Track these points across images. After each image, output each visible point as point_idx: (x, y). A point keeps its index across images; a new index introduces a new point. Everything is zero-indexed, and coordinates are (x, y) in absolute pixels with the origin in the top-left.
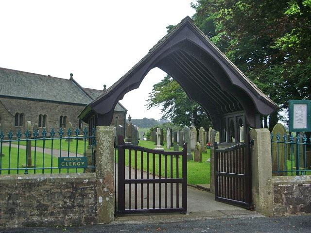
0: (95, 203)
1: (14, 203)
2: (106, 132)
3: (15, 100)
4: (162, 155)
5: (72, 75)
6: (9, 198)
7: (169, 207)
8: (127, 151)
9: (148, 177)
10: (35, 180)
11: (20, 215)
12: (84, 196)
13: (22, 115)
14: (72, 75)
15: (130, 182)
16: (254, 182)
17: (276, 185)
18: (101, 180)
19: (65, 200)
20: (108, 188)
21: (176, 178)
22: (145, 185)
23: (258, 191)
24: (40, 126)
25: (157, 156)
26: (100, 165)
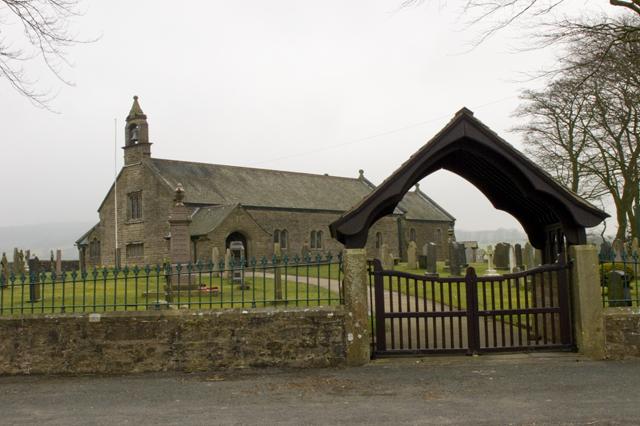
0: (344, 342)
1: (238, 341)
2: (354, 256)
3: (272, 212)
4: (436, 283)
5: (361, 172)
6: (233, 335)
7: (448, 347)
8: (386, 279)
9: (443, 309)
10: (264, 314)
11: (246, 354)
12: (328, 333)
13: (283, 233)
14: (361, 172)
15: (392, 316)
16: (576, 316)
17: (608, 319)
18: (350, 314)
19: (304, 337)
20: (360, 323)
21: (549, 307)
22: (439, 320)
23: (581, 327)
24: (312, 247)
25: (488, 284)
26: (349, 296)
